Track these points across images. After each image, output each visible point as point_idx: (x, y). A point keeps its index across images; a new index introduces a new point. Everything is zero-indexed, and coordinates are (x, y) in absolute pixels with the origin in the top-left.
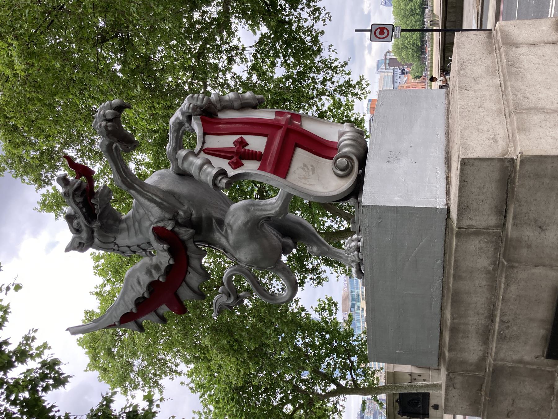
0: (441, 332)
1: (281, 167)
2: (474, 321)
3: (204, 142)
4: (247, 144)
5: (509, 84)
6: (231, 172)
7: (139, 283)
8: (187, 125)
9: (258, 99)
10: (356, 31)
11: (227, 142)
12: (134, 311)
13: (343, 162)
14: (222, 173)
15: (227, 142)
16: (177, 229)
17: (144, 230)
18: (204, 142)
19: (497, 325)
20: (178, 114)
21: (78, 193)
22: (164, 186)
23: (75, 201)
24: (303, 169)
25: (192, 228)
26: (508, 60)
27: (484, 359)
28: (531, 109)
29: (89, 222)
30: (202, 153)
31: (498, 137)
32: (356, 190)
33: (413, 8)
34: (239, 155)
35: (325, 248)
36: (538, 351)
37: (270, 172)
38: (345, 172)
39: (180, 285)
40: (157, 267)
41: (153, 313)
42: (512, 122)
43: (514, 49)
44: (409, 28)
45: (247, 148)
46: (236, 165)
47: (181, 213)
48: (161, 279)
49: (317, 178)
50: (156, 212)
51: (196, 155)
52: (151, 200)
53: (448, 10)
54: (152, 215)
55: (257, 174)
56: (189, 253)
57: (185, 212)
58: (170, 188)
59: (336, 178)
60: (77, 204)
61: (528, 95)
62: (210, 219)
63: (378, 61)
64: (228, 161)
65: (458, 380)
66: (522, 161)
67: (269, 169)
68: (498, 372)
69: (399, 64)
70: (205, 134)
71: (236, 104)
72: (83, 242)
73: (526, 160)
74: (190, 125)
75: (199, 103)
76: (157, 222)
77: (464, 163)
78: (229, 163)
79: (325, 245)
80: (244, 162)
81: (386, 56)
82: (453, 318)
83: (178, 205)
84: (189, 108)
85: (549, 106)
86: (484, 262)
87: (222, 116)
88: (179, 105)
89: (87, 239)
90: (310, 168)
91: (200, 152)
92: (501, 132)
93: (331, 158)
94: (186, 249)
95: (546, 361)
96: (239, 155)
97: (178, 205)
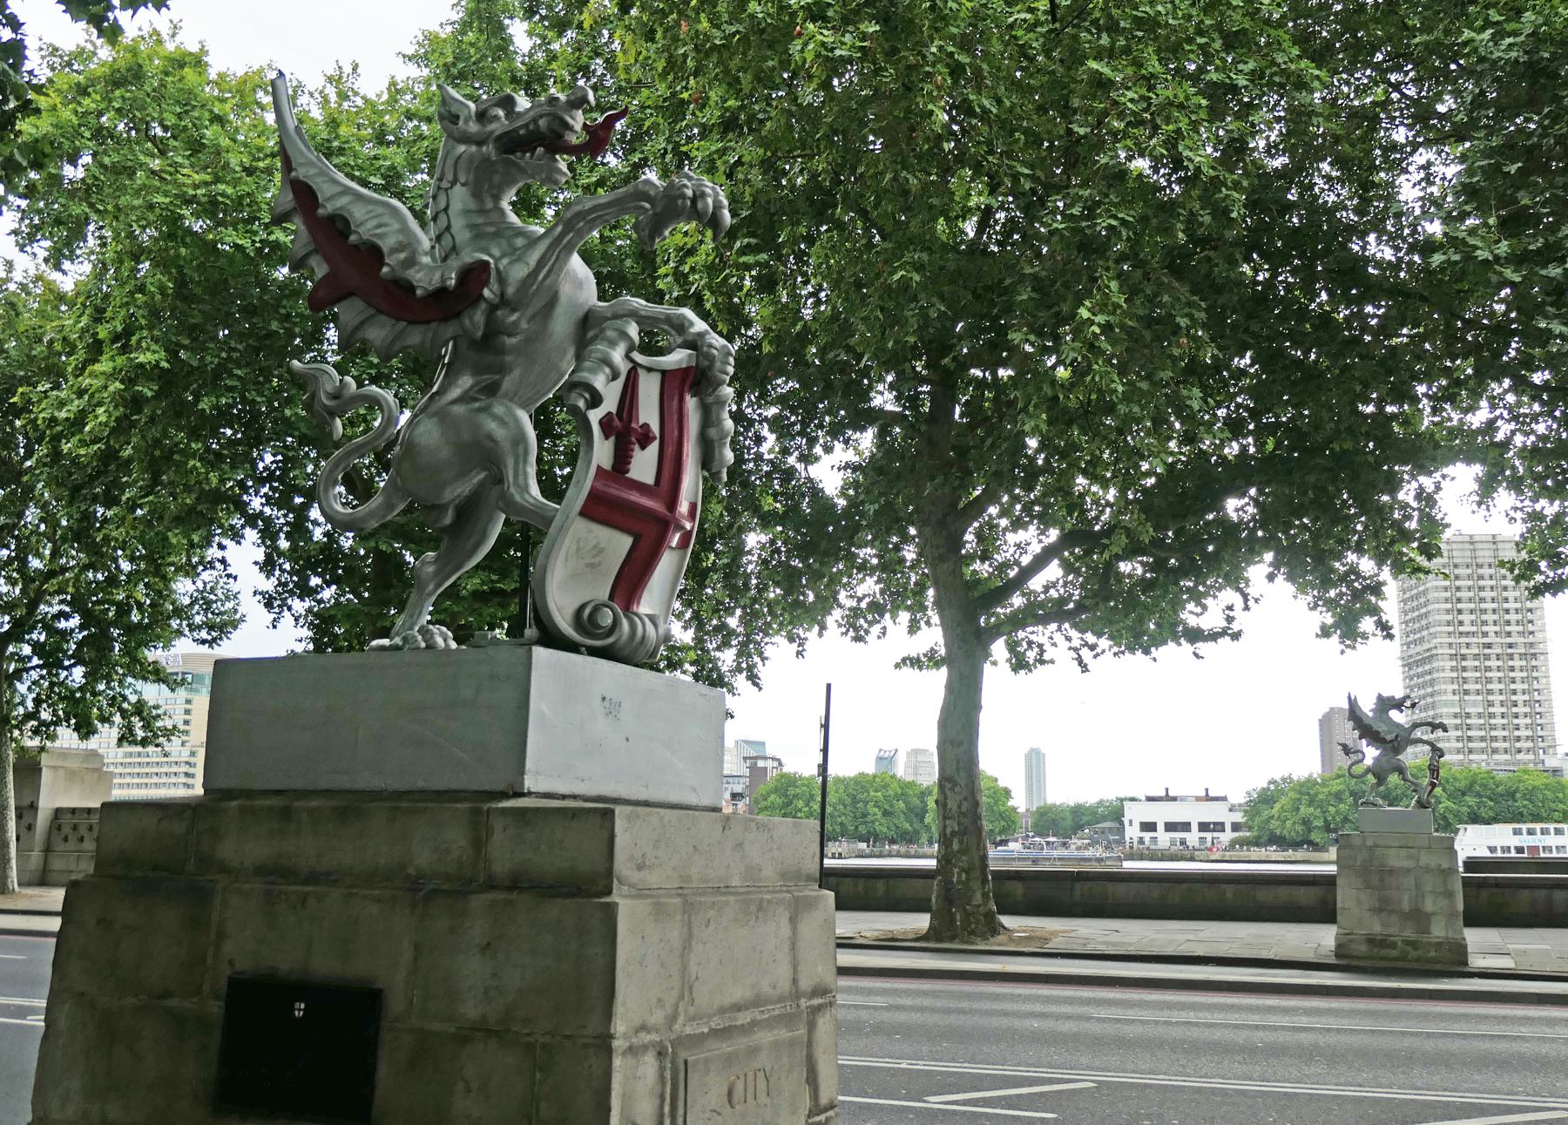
0: (278, 792)
1: (600, 509)
2: (306, 849)
3: (649, 370)
4: (643, 448)
5: (732, 898)
6: (595, 416)
7: (379, 226)
8: (679, 340)
9: (719, 472)
10: (829, 686)
11: (648, 414)
12: (320, 211)
13: (606, 618)
14: (595, 400)
15: (648, 414)
16: (483, 306)
17: (483, 243)
18: (649, 370)
19: (299, 888)
20: (700, 326)
21: (556, 127)
22: (565, 289)
23: (541, 116)
24: (595, 547)
25: (485, 335)
26: (769, 902)
27: (225, 869)
28: (690, 929)
29: (500, 137)
30: (630, 365)
31: (645, 872)
32: (552, 639)
33: (870, 818)
34: (624, 431)
35: (431, 587)
36: (244, 965)
37: (593, 489)
38: (585, 620)
39: (369, 304)
40: (411, 262)
41: (312, 248)
42: (671, 896)
43: (787, 915)
44: (829, 809)
45: (637, 447)
46: (606, 424)
47: (514, 317)
48: (385, 269)
49: (572, 574)
50: (519, 272)
51: (628, 357)
52: (541, 263)
53: (862, 881)
54: (510, 263)
55: (590, 462)
56: (434, 325)
57: (516, 323)
58: (563, 299)
59: (576, 605)
60: (535, 121)
61: (712, 927)
62: (503, 370)
63: (763, 744)
64: (614, 411)
65: (178, 827)
66: (608, 904)
67: (599, 486)
68: (200, 897)
69: (751, 786)
70: (664, 373)
71: (712, 432)
72: (461, 122)
73: (610, 912)
74: (679, 347)
75: (718, 364)
76: (497, 269)
77: (613, 811)
78: (609, 413)
79: (438, 586)
80: (612, 439)
81: (773, 759)
82: (311, 811)
83: (530, 311)
84: (710, 346)
85: (693, 958)
86: (423, 858)
87: (691, 403)
88: (714, 327)
89: (465, 132)
90: (596, 560)
91: (632, 360)
92: (653, 879)
93: (611, 598)
94: (445, 319)
95: (223, 982)
96: (624, 431)
97: (530, 311)
